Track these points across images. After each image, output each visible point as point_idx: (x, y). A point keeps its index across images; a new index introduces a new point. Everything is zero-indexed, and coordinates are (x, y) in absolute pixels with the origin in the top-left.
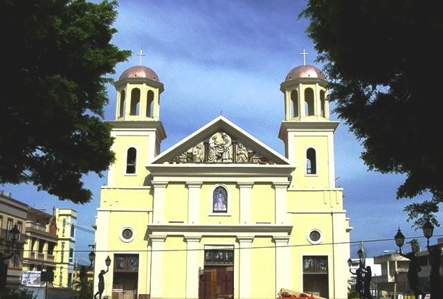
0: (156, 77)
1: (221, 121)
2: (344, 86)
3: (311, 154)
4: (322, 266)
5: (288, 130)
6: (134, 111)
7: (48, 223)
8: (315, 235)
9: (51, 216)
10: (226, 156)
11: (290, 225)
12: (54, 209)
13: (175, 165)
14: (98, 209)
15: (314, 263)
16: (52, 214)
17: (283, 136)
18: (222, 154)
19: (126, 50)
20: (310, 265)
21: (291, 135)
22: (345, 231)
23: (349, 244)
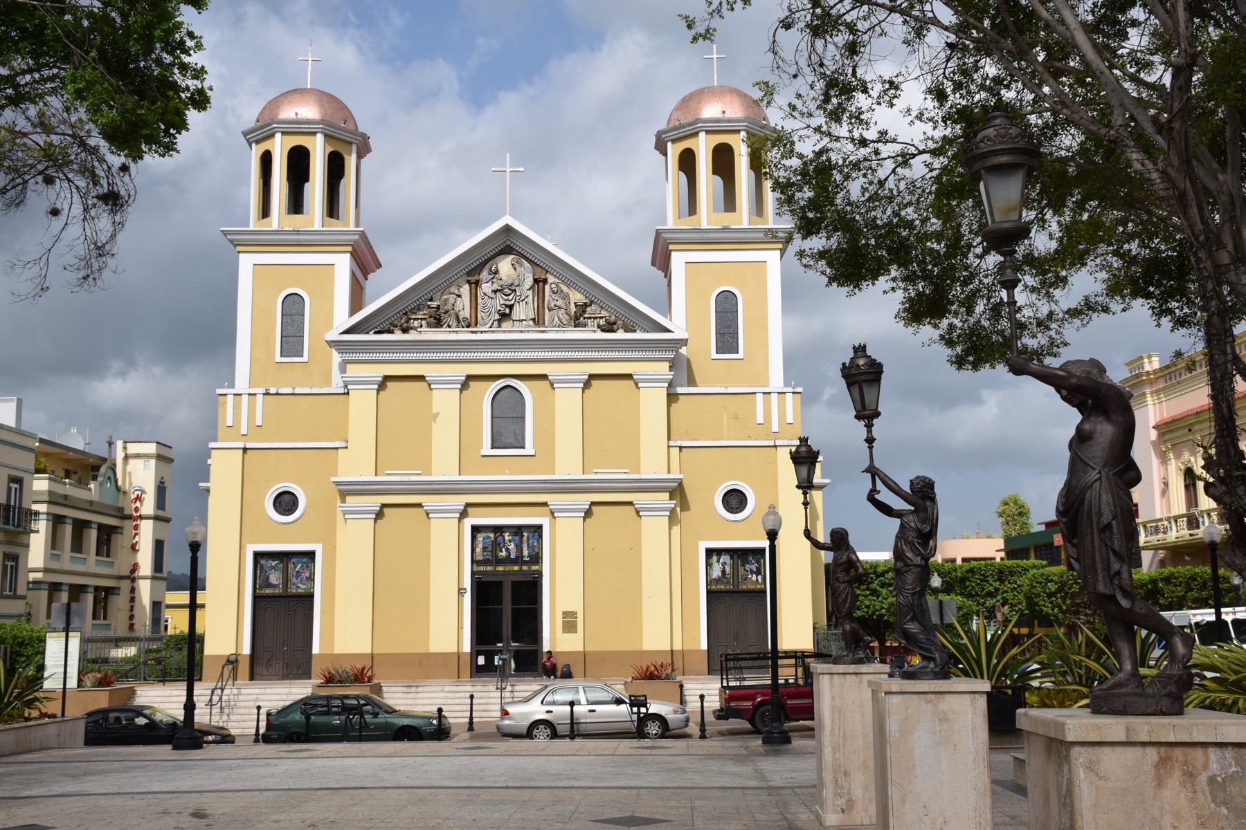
0: (348, 116)
1: (507, 229)
2: (920, 295)
3: (727, 307)
4: (752, 572)
5: (671, 247)
6: (296, 204)
7: (95, 478)
8: (735, 500)
9: (105, 460)
10: (520, 312)
11: (167, 508)
12: (110, 444)
13: (398, 336)
14: (212, 445)
15: (733, 567)
16: (105, 455)
17: (662, 260)
18: (511, 307)
19: (883, 376)
20: (724, 572)
21: (679, 260)
22: (206, 606)
23: (369, 651)
